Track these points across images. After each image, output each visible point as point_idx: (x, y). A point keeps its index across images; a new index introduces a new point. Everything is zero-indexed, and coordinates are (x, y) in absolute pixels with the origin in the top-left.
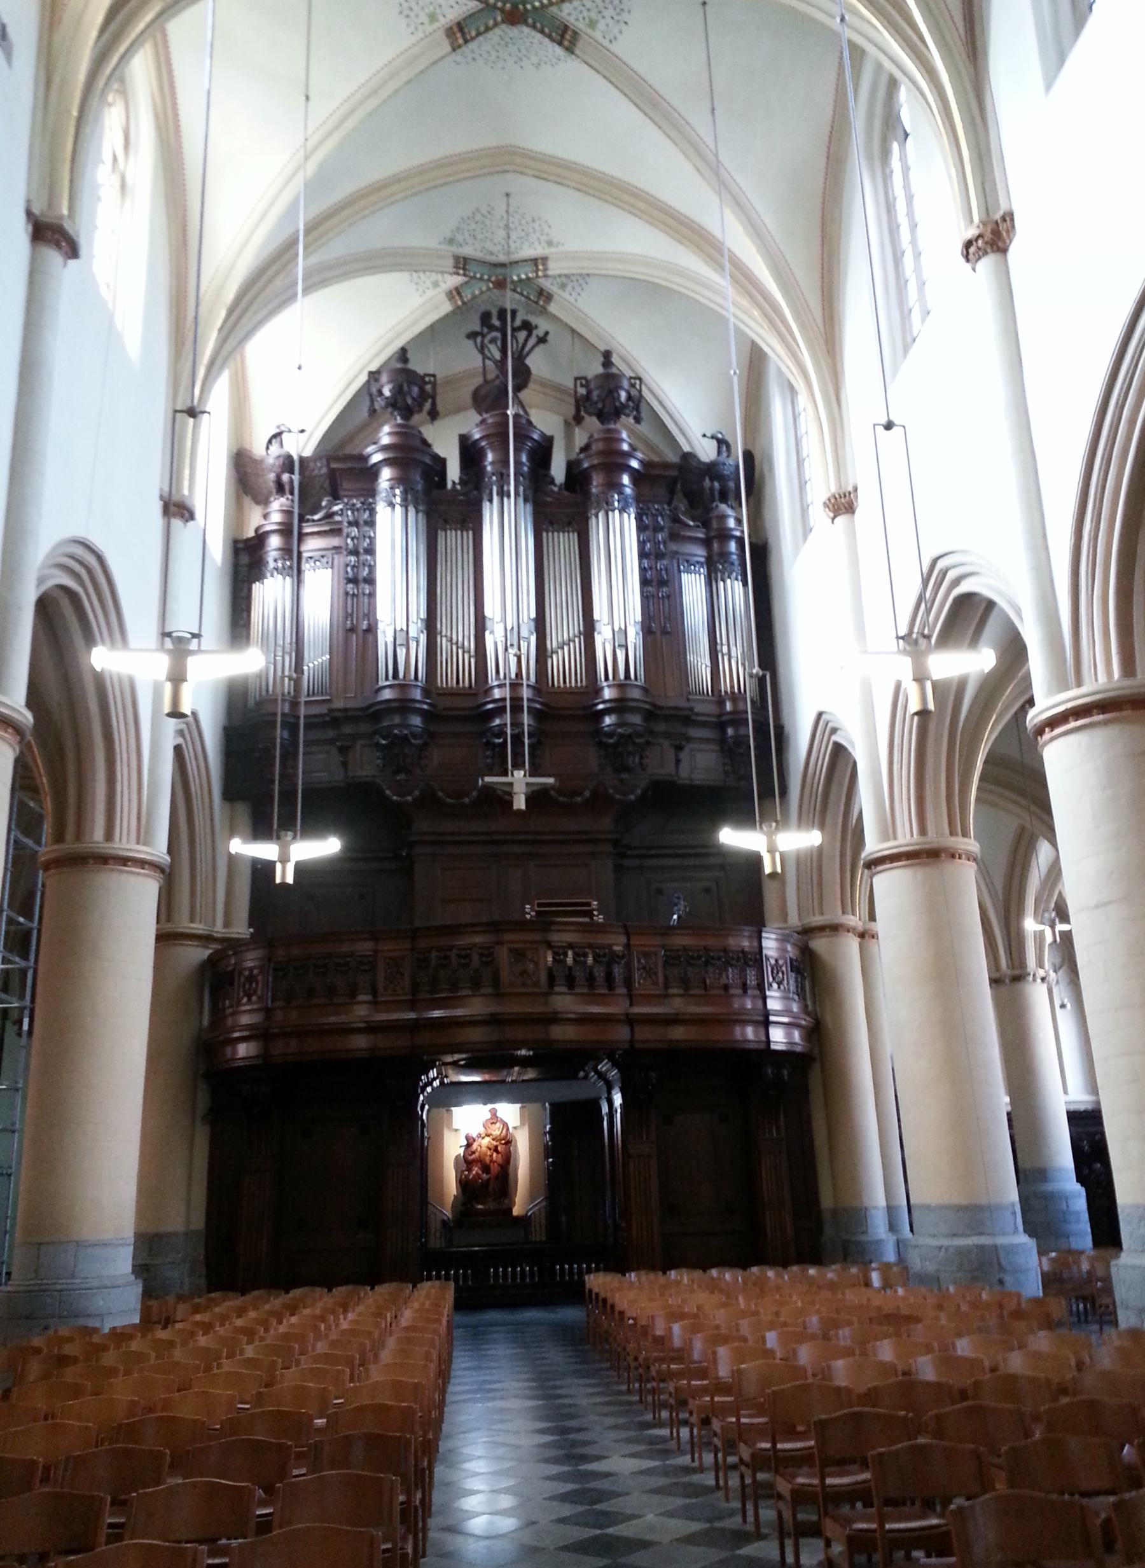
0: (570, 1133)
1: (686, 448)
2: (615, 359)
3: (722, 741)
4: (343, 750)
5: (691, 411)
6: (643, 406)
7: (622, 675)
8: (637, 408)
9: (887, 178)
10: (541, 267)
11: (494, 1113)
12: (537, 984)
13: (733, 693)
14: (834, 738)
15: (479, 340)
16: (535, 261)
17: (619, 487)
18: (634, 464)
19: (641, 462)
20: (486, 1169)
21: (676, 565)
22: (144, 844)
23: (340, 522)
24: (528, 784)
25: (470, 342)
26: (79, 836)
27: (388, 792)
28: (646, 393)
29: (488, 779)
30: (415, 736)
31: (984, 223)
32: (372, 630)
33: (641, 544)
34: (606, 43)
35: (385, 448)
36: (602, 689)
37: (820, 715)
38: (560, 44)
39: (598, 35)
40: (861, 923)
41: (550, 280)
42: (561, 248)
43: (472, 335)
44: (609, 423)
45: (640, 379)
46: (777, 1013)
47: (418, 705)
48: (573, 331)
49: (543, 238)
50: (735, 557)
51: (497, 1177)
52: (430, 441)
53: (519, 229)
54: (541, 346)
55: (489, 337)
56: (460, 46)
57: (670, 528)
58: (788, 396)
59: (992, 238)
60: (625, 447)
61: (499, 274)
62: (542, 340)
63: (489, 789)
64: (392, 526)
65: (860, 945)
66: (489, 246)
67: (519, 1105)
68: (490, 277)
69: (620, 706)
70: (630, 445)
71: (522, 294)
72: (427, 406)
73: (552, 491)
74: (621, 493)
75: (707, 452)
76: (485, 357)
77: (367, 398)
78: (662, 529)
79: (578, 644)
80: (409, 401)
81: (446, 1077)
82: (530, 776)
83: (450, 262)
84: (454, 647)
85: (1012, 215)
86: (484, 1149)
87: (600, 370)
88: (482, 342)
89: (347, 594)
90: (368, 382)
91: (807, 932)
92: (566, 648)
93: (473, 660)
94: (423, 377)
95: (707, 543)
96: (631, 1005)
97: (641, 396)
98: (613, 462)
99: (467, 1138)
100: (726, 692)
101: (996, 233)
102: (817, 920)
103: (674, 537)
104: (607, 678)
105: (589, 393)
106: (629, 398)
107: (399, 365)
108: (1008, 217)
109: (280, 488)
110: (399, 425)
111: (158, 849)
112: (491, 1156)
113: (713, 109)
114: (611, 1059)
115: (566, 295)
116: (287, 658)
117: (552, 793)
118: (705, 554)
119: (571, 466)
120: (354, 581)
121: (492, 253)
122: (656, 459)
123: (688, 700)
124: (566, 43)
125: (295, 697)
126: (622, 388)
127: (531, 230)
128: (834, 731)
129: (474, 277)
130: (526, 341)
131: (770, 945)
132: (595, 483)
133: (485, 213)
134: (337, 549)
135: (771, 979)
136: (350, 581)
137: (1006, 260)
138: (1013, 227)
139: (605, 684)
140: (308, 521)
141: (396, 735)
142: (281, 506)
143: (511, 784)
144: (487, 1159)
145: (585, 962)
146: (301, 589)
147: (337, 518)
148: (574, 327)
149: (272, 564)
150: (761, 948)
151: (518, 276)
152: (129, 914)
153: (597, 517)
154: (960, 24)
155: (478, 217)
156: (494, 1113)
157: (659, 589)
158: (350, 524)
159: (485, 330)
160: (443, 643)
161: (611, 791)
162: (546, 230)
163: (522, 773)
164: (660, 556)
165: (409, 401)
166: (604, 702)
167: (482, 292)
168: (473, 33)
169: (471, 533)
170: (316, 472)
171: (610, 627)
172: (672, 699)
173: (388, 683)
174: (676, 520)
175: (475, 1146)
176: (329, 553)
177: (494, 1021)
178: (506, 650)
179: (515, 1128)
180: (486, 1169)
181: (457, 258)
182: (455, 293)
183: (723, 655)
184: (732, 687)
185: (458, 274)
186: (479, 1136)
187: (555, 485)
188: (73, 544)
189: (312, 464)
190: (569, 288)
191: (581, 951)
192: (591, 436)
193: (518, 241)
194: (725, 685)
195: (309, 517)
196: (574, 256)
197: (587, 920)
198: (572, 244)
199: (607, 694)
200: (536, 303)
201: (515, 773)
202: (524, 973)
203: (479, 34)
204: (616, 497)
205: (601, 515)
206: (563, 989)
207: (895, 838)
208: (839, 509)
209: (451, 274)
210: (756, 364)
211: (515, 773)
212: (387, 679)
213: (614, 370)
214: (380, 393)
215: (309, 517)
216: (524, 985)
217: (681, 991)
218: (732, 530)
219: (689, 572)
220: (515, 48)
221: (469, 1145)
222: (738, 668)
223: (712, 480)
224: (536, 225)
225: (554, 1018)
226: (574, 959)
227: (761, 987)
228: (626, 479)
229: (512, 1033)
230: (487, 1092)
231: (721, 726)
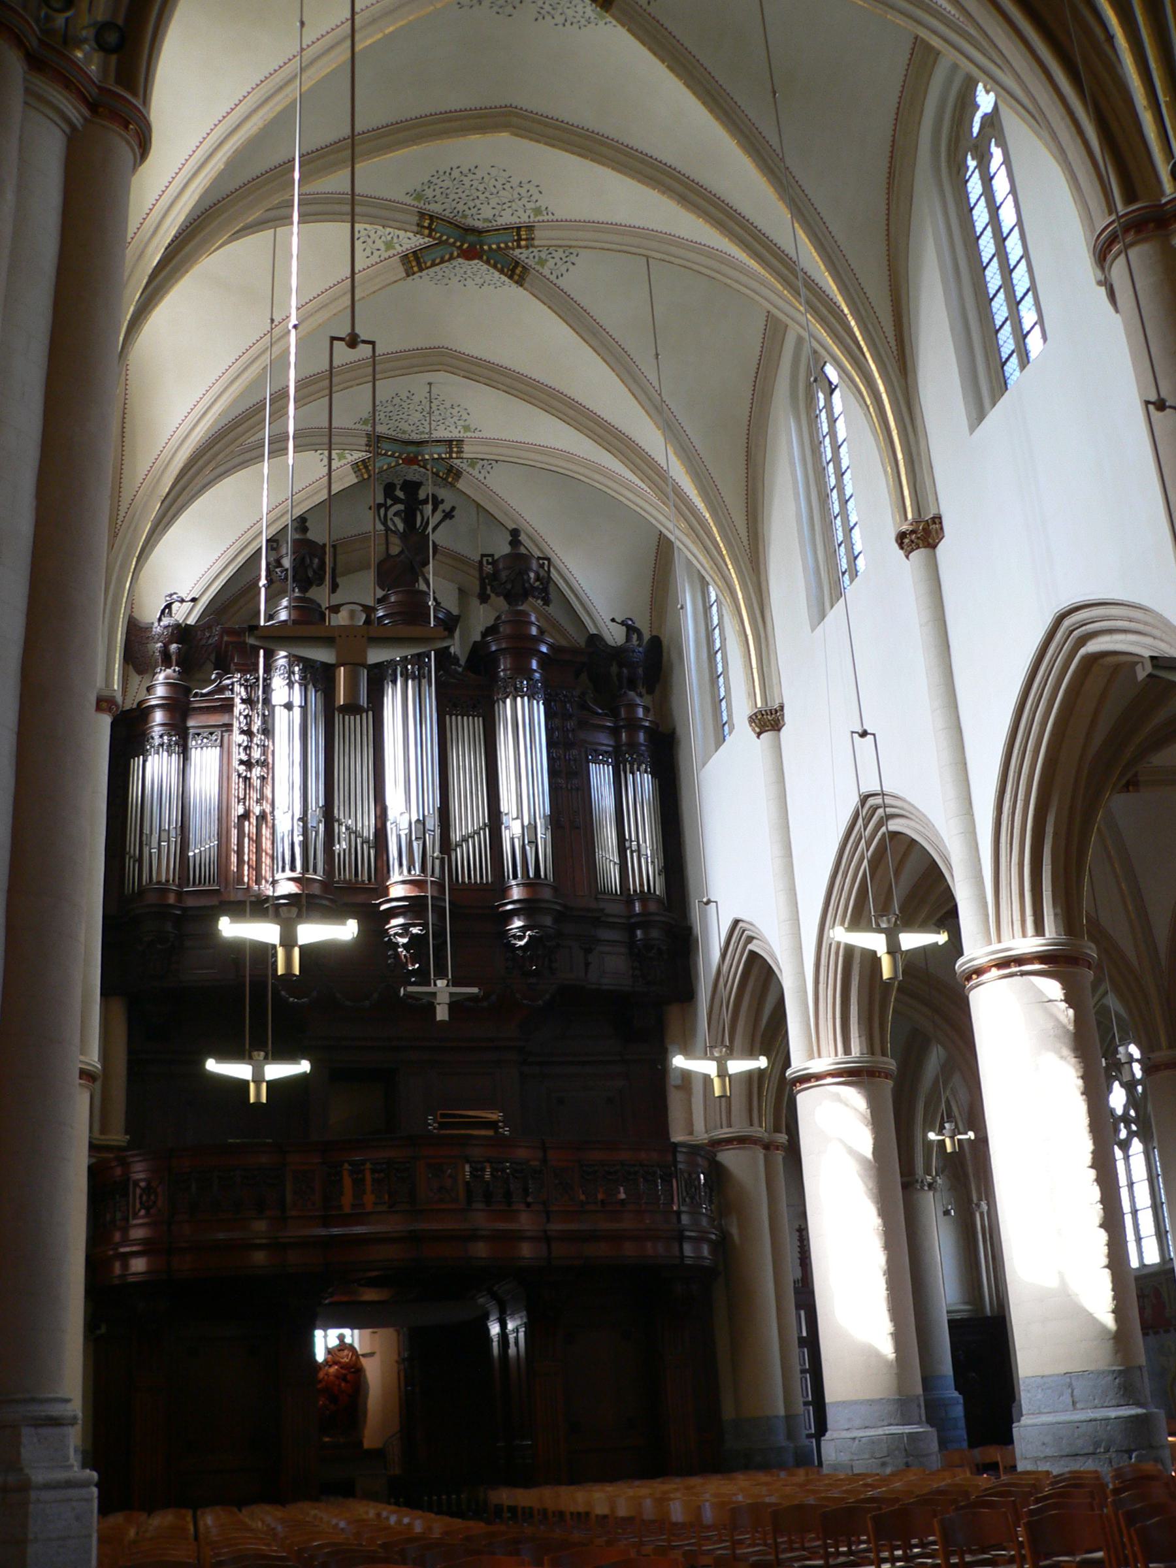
1: (593, 630)
2: (523, 538)
3: (631, 943)
5: (597, 589)
6: (552, 588)
7: (531, 875)
8: (545, 590)
9: (813, 420)
13: (642, 891)
14: (750, 947)
16: (450, 442)
17: (528, 673)
24: (451, 994)
27: (283, 993)
28: (554, 574)
31: (916, 522)
34: (553, 278)
37: (736, 922)
38: (511, 277)
39: (546, 272)
40: (766, 1135)
44: (517, 605)
45: (548, 559)
48: (478, 505)
54: (448, 521)
56: (414, 273)
58: (698, 587)
59: (922, 535)
60: (534, 631)
61: (411, 450)
62: (449, 515)
65: (766, 1156)
66: (404, 426)
68: (401, 454)
70: (539, 627)
73: (457, 672)
74: (530, 679)
75: (615, 635)
78: (571, 716)
80: (310, 574)
84: (353, 836)
85: (940, 518)
87: (506, 549)
88: (386, 515)
93: (372, 852)
95: (615, 732)
96: (548, 1221)
97: (549, 577)
98: (522, 647)
100: (635, 891)
101: (926, 531)
103: (583, 725)
104: (515, 877)
106: (538, 578)
108: (937, 519)
109: (167, 661)
110: (297, 599)
112: (339, 1385)
113: (657, 355)
115: (475, 473)
118: (612, 743)
121: (404, 432)
122: (564, 643)
123: (596, 899)
124: (516, 277)
128: (750, 939)
133: (405, 398)
137: (935, 555)
138: (942, 529)
139: (513, 882)
142: (167, 678)
143: (434, 994)
145: (482, 1177)
146: (188, 768)
148: (482, 503)
149: (157, 741)
151: (431, 455)
153: (505, 703)
154: (893, 343)
155: (397, 401)
159: (389, 502)
161: (518, 996)
162: (465, 416)
163: (445, 982)
164: (569, 745)
165: (310, 574)
167: (390, 467)
168: (429, 264)
170: (203, 642)
171: (519, 821)
174: (583, 706)
179: (363, 1355)
183: (632, 852)
184: (642, 885)
191: (479, 1166)
192: (498, 618)
194: (633, 884)
196: (486, 442)
197: (490, 1133)
198: (490, 431)
199: (516, 893)
200: (446, 479)
201: (439, 983)
203: (433, 265)
205: (508, 701)
206: (481, 1206)
208: (765, 725)
210: (663, 550)
213: (523, 550)
219: (596, 762)
220: (462, 271)
222: (646, 867)
223: (620, 665)
224: (454, 412)
226: (491, 1174)
231: (631, 929)
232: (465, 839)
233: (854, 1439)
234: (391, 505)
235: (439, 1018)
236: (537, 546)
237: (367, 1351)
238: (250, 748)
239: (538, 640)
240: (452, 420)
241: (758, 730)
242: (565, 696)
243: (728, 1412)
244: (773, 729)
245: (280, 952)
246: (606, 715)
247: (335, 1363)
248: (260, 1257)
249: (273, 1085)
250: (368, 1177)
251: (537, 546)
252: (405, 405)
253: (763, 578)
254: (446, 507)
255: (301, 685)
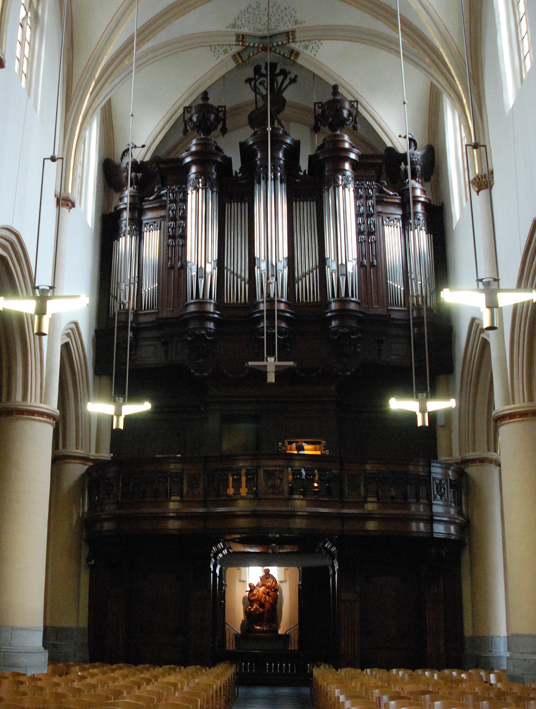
0: (311, 587)
1: (389, 145)
2: (341, 90)
4: (165, 344)
7: (343, 295)
10: (291, 37)
11: (267, 572)
12: (282, 493)
14: (482, 335)
15: (253, 83)
16: (287, 33)
17: (342, 171)
18: (353, 156)
19: (357, 154)
20: (262, 605)
21: (381, 221)
22: (44, 403)
23: (165, 201)
24: (276, 366)
25: (248, 85)
26: (9, 398)
28: (360, 109)
29: (251, 363)
30: (209, 335)
32: (184, 267)
33: (357, 208)
35: (192, 154)
36: (330, 303)
41: (298, 44)
42: (303, 25)
43: (248, 81)
45: (357, 102)
46: (439, 515)
47: (211, 315)
49: (292, 19)
50: (420, 215)
51: (268, 611)
52: (221, 147)
53: (277, 15)
54: (293, 85)
55: (259, 81)
57: (377, 197)
60: (347, 146)
62: (293, 81)
63: (253, 370)
64: (197, 204)
67: (284, 568)
69: (343, 314)
70: (350, 144)
71: (280, 54)
72: (220, 126)
75: (402, 146)
76: (256, 93)
77: (183, 123)
78: (371, 198)
79: (316, 273)
81: (230, 548)
82: (279, 360)
83: (234, 38)
86: (260, 593)
87: (331, 97)
88: (255, 84)
89: (169, 245)
90: (184, 113)
91: (466, 462)
92: (307, 277)
94: (217, 109)
97: (358, 111)
99: (250, 585)
102: (471, 455)
103: (380, 202)
105: (323, 111)
106: (350, 114)
107: (201, 102)
111: (52, 405)
112: (265, 598)
114: (331, 541)
115: (308, 52)
116: (132, 287)
117: (297, 371)
119: (311, 159)
120: (173, 237)
121: (260, 31)
125: (136, 311)
126: (344, 108)
127: (284, 15)
129: (249, 46)
130: (283, 82)
131: (437, 471)
132: (327, 169)
134: (163, 217)
135: (436, 493)
136: (170, 237)
139: (332, 300)
140: (146, 201)
141: (196, 334)
143: (266, 366)
144: (263, 600)
147: (164, 198)
150: (430, 472)
152: (36, 445)
153: (328, 191)
155: (251, 10)
156: (267, 572)
157: (369, 236)
158: (171, 202)
160: (228, 275)
163: (273, 359)
164: (370, 215)
166: (331, 311)
169: (247, 204)
172: (377, 310)
173: (193, 301)
174: (381, 191)
175: (255, 592)
176: (158, 221)
177: (254, 515)
178: (268, 279)
179: (281, 582)
180: (262, 605)
181: (238, 36)
182: (237, 56)
185: (239, 45)
186: (258, 585)
187: (301, 171)
188: (5, 230)
189: (149, 166)
190: (311, 47)
192: (325, 139)
193: (277, 22)
195: (146, 198)
199: (333, 306)
200: (290, 58)
202: (273, 486)
204: (340, 177)
207: (514, 403)
209: (236, 45)
211: (269, 359)
212: (192, 298)
214: (191, 119)
215: (146, 198)
216: (273, 493)
217: (375, 499)
218: (418, 197)
221: (251, 591)
225: (293, 515)
227: (429, 498)
228: (347, 166)
229: (266, 523)
230: (264, 559)
232: (304, 276)
233: (525, 660)
234: (258, 79)
235: (269, 380)
236: (351, 94)
237: (282, 579)
238: (175, 229)
239: (348, 151)
240: (287, 19)
241: (477, 189)
242: (368, 185)
243: (468, 632)
244: (487, 188)
245: (36, 317)
246: (396, 195)
247: (263, 585)
248: (371, 526)
249: (128, 419)
250: (244, 479)
251: (351, 94)
252: (256, 12)
253: (481, 88)
254: (292, 76)
255: (202, 189)
